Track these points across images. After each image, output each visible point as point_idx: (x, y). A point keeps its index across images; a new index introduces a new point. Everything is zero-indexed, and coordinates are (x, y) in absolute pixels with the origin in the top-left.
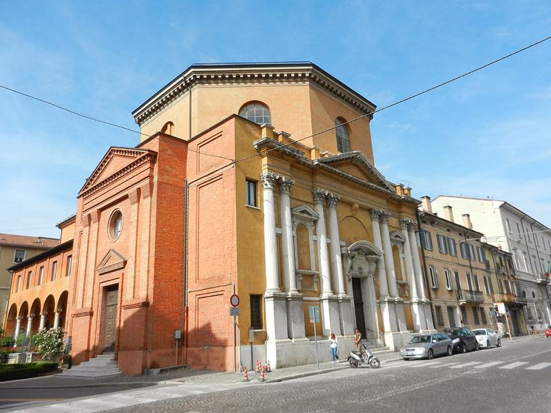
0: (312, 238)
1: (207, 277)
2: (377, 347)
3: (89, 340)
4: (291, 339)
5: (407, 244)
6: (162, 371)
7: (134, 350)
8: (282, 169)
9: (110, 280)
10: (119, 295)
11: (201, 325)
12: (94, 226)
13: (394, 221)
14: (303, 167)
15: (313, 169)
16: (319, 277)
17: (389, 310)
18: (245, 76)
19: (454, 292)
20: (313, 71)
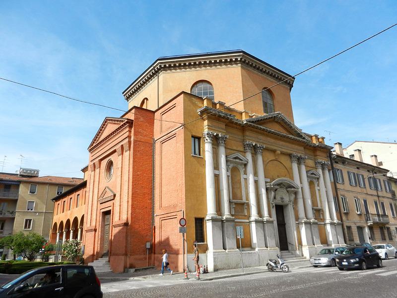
0: (243, 176)
1: (167, 205)
2: (296, 257)
3: (94, 248)
4: (267, 248)
5: (322, 179)
6: (136, 271)
7: (118, 255)
8: (219, 128)
9: (106, 207)
10: (111, 218)
11: (163, 239)
12: (97, 171)
13: (311, 163)
14: (235, 126)
15: (243, 126)
16: (248, 205)
17: (306, 229)
18: (195, 63)
19: (363, 215)
20: (243, 56)
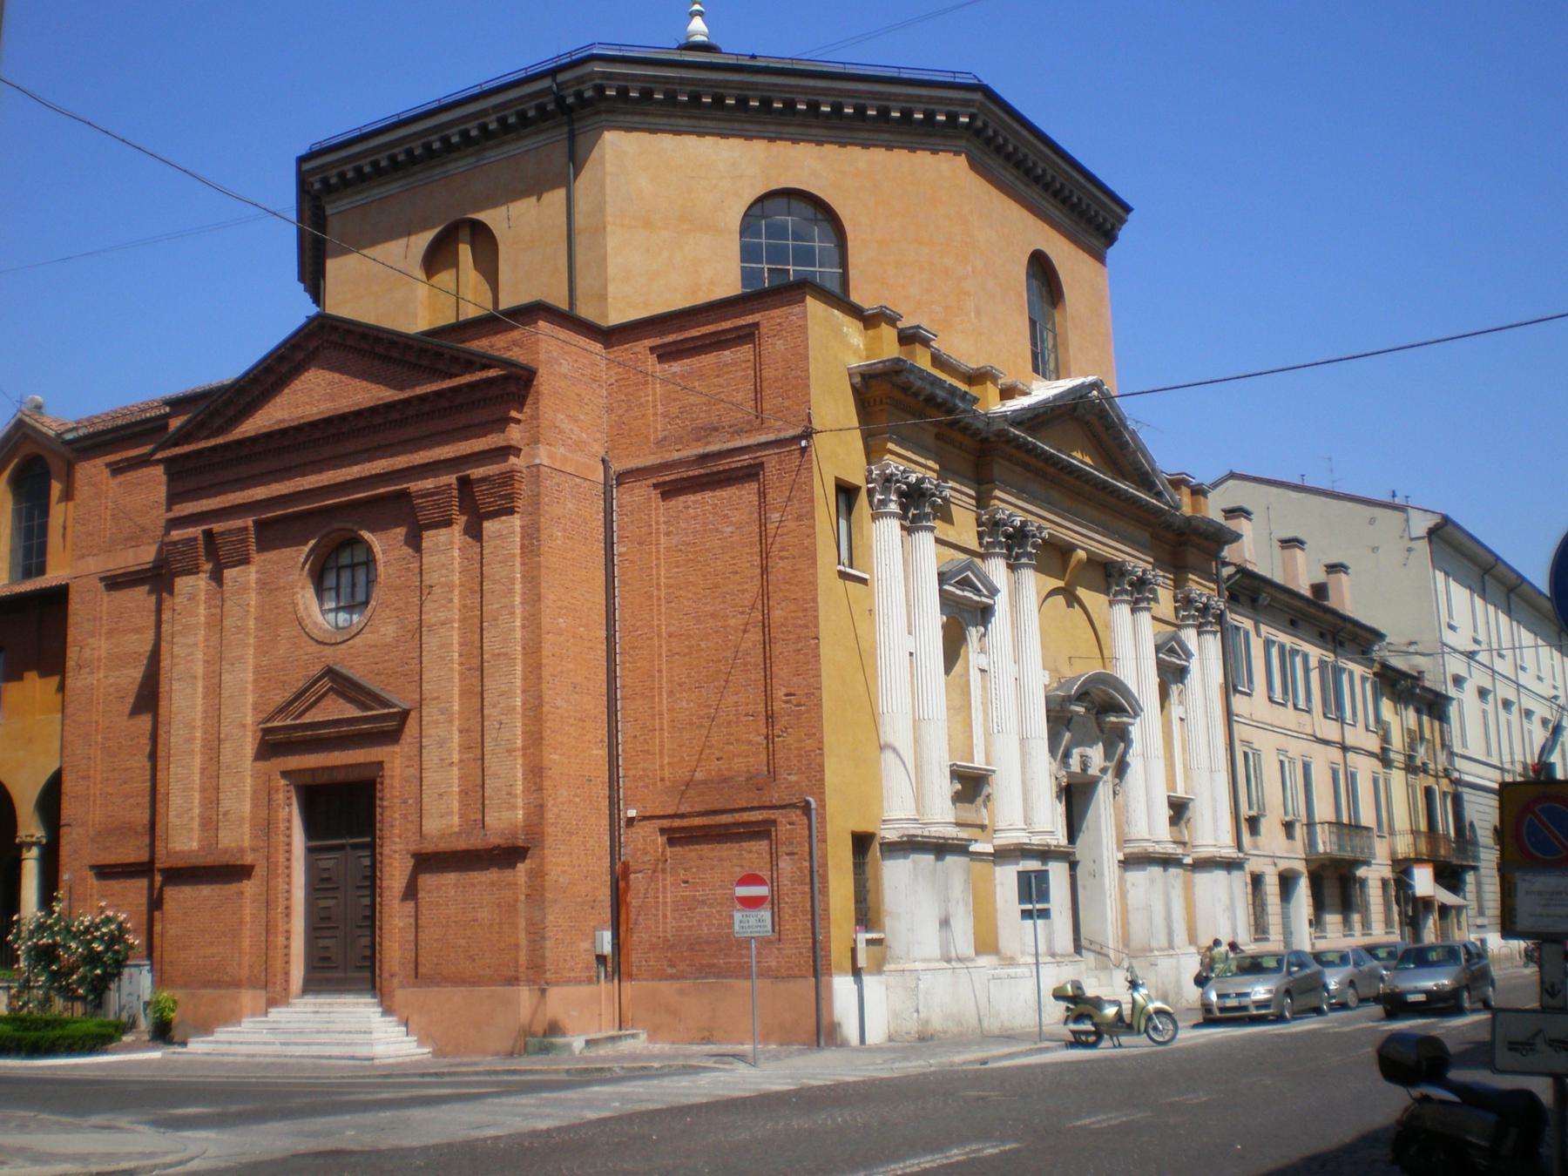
15: (985, 441)
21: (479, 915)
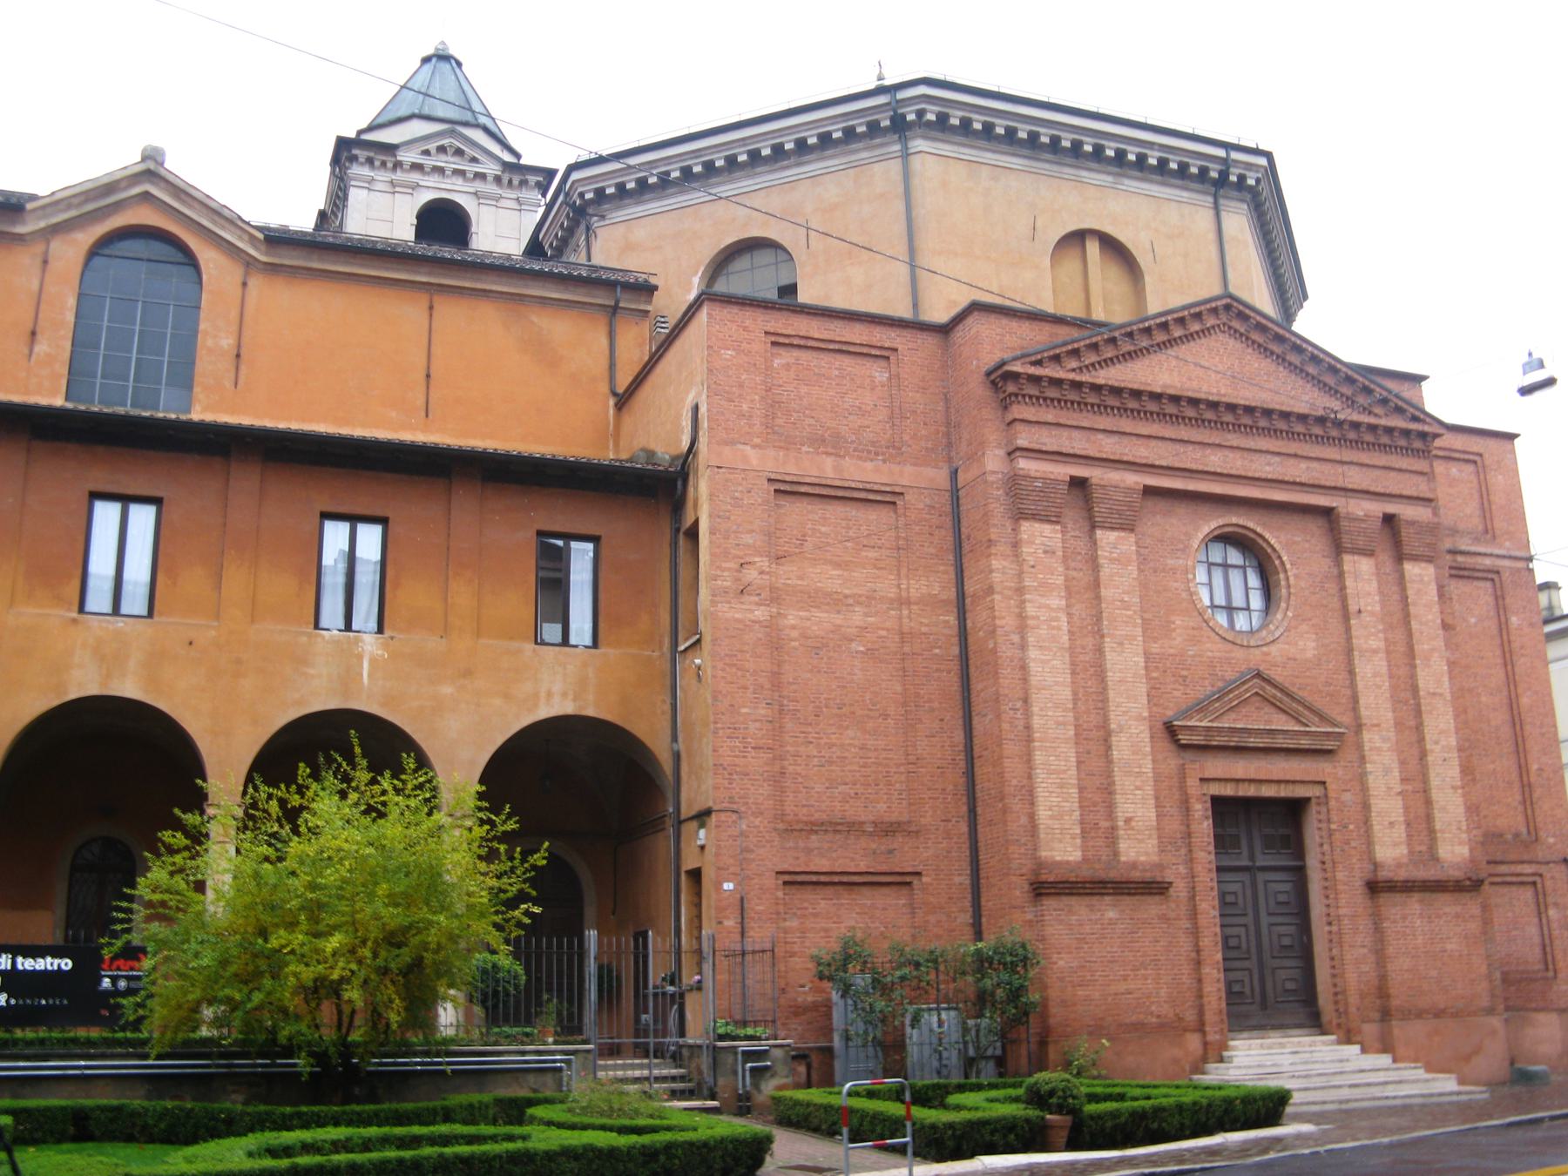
21: (1449, 947)
